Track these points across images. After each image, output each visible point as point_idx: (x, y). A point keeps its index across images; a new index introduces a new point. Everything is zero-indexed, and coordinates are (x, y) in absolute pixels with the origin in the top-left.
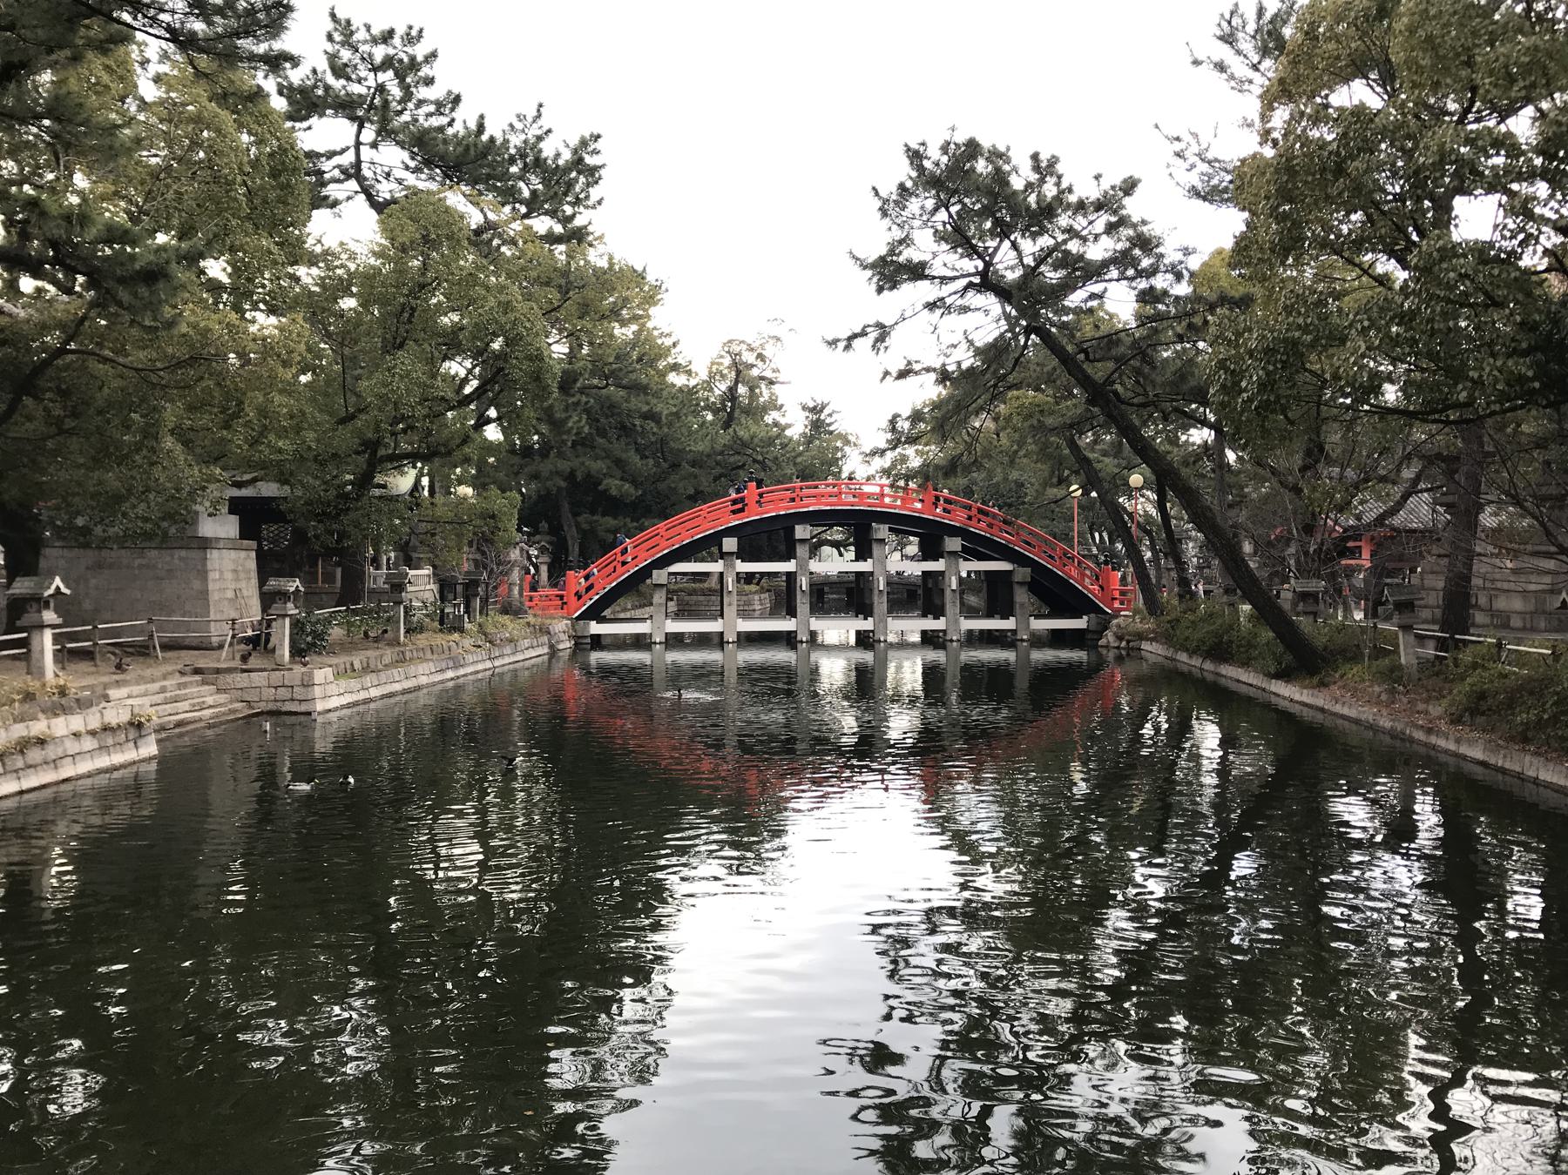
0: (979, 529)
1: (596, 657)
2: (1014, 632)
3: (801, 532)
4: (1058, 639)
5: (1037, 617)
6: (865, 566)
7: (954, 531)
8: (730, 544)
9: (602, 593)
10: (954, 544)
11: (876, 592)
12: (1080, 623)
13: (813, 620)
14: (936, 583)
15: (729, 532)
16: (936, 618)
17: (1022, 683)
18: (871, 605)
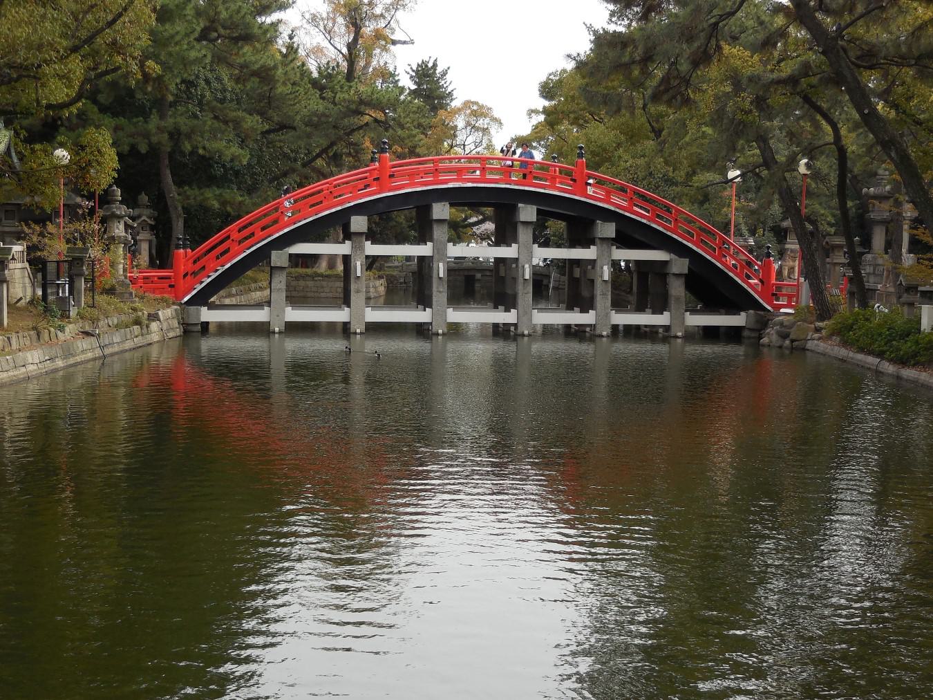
0: (640, 214)
2: (667, 328)
3: (441, 211)
4: (710, 334)
5: (694, 311)
6: (425, 250)
7: (608, 215)
8: (359, 223)
9: (214, 275)
11: (521, 280)
12: (738, 320)
13: (450, 311)
14: (585, 272)
16: (508, 310)
18: (430, 297)
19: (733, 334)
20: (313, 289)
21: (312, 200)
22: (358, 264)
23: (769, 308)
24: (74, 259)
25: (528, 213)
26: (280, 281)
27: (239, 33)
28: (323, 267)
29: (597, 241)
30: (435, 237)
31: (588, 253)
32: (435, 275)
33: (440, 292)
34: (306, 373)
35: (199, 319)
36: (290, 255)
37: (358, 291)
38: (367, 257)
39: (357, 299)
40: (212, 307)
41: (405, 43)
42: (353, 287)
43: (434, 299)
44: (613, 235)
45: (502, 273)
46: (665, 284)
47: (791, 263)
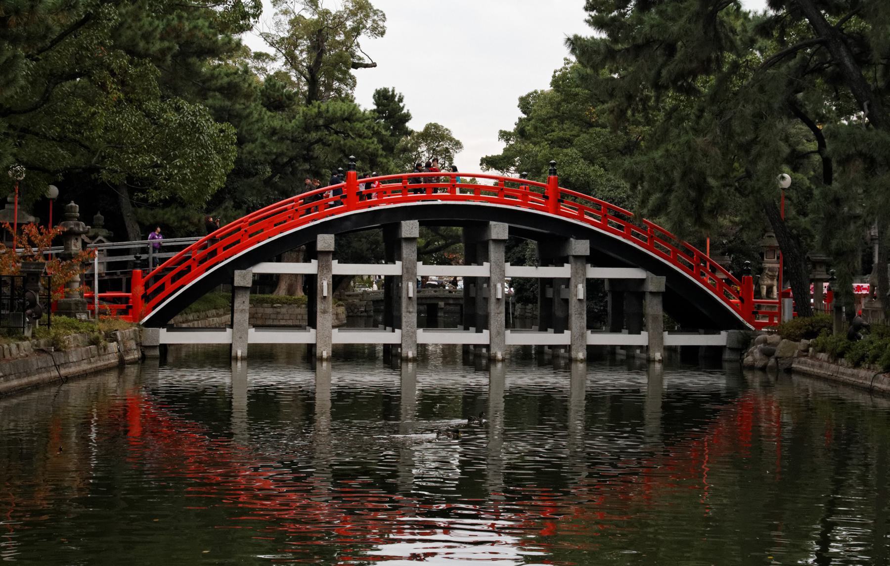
1: (165, 378)
4: (689, 358)
5: (672, 331)
6: (394, 269)
7: (582, 233)
8: (326, 242)
10: (581, 247)
11: (493, 300)
12: (719, 339)
14: (558, 292)
15: (325, 228)
16: (479, 331)
17: (653, 410)
19: (710, 358)
20: (273, 316)
21: (277, 218)
22: (325, 284)
23: (751, 327)
24: (30, 274)
25: (499, 230)
26: (242, 303)
27: (194, 55)
28: (282, 292)
29: (571, 259)
30: (404, 255)
31: (563, 272)
32: (404, 295)
33: (410, 312)
34: (264, 402)
35: (158, 341)
36: (254, 275)
37: (324, 312)
38: (334, 277)
39: (325, 320)
40: (171, 329)
41: (366, 66)
42: (320, 306)
43: (404, 320)
44: (588, 253)
45: (473, 294)
46: (641, 306)
47: (769, 282)
